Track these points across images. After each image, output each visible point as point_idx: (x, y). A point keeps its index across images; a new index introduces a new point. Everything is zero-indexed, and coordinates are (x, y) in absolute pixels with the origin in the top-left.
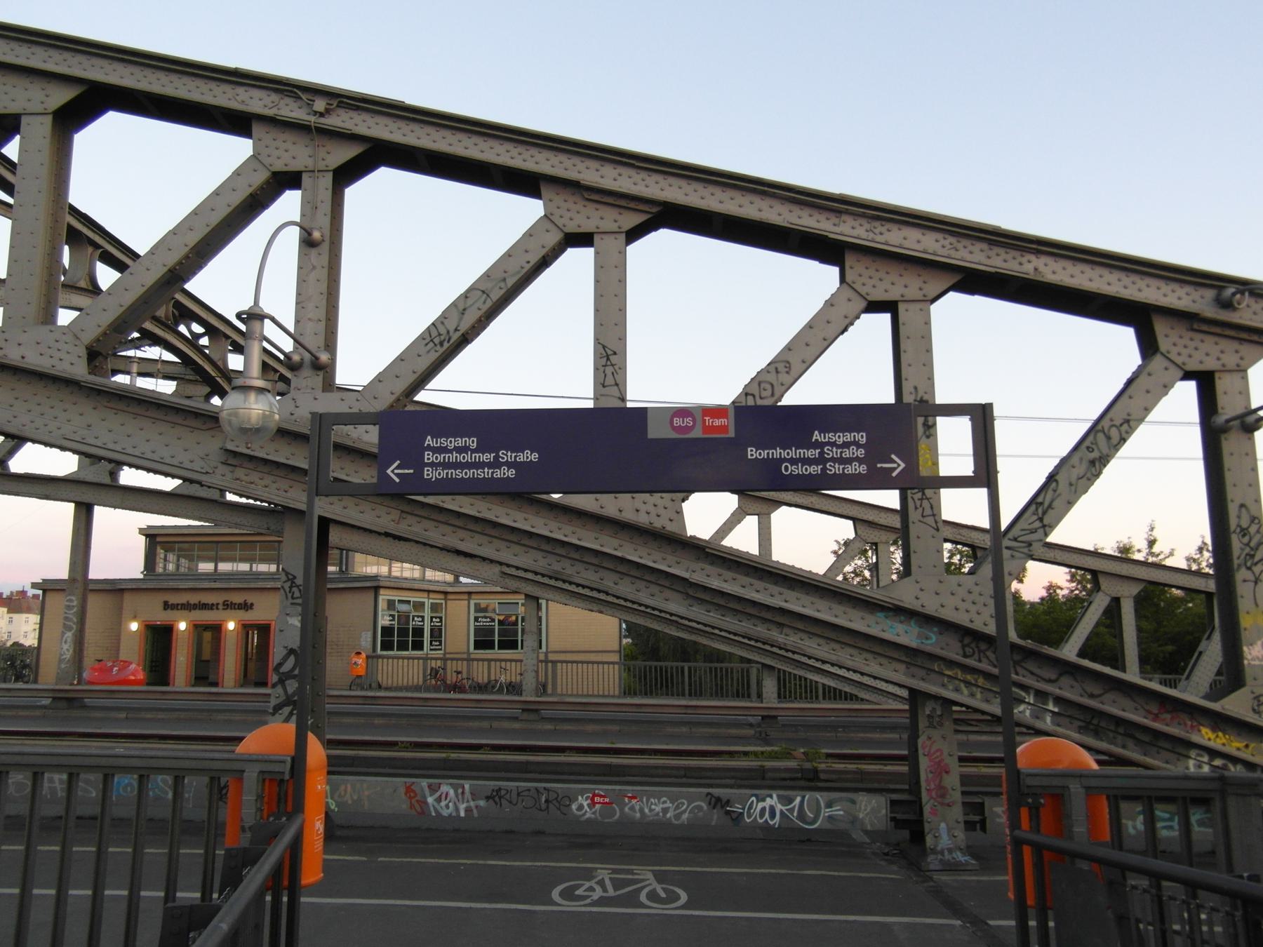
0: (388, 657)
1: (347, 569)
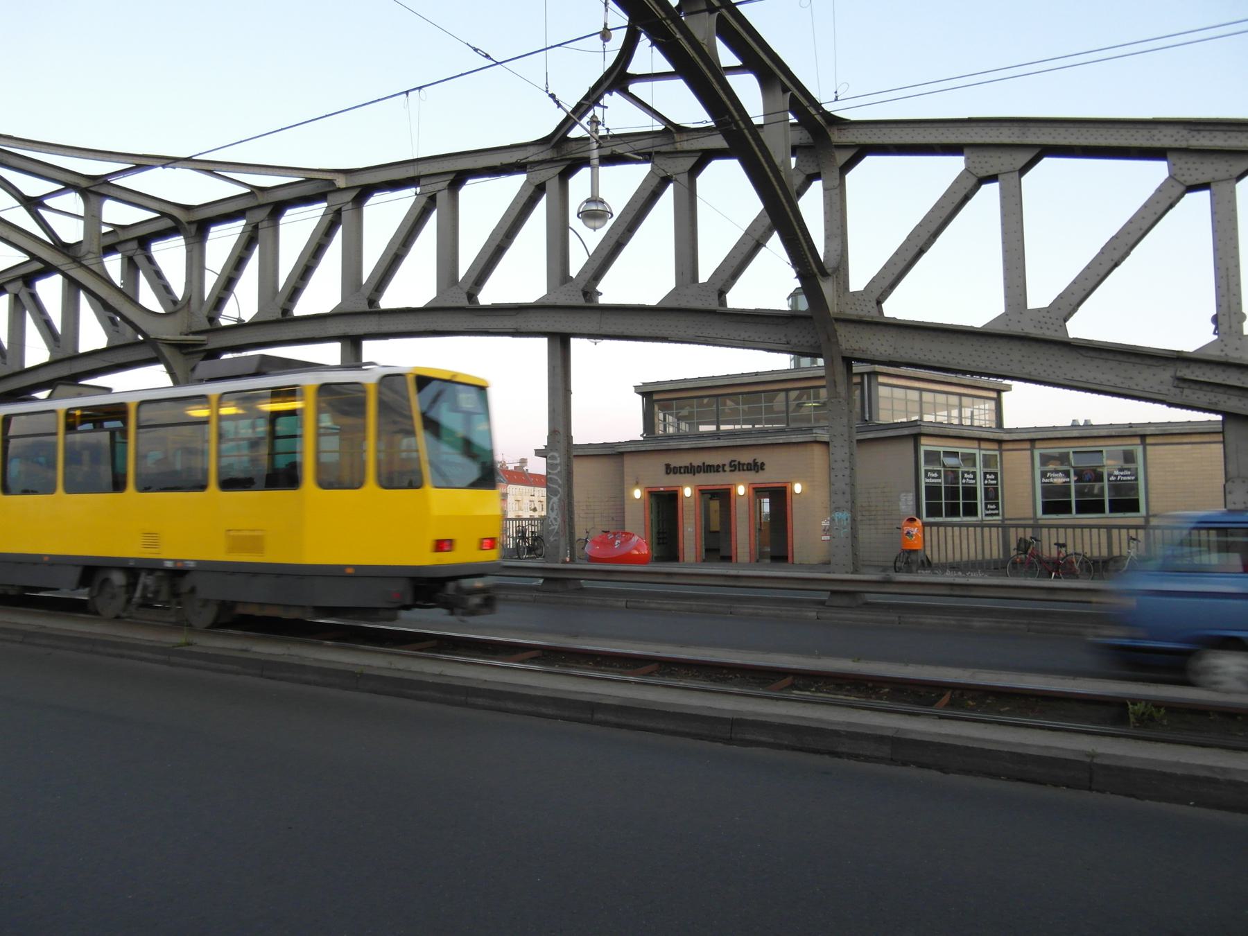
0: (953, 525)
1: (870, 417)
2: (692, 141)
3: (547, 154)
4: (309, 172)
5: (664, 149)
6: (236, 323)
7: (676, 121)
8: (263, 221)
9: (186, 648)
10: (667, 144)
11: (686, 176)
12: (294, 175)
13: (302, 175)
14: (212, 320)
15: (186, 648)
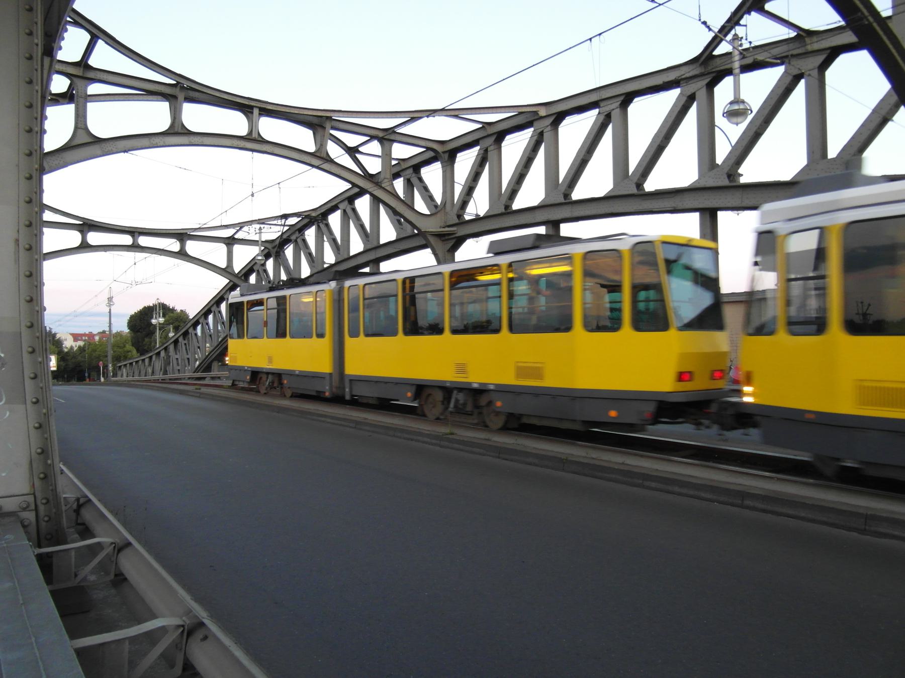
2: (823, 42)
3: (697, 71)
4: (521, 108)
5: (795, 52)
6: (475, 217)
7: (806, 26)
8: (490, 146)
9: (451, 436)
10: (798, 48)
11: (816, 71)
12: (511, 111)
13: (517, 110)
14: (460, 216)
15: (451, 436)
